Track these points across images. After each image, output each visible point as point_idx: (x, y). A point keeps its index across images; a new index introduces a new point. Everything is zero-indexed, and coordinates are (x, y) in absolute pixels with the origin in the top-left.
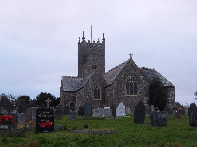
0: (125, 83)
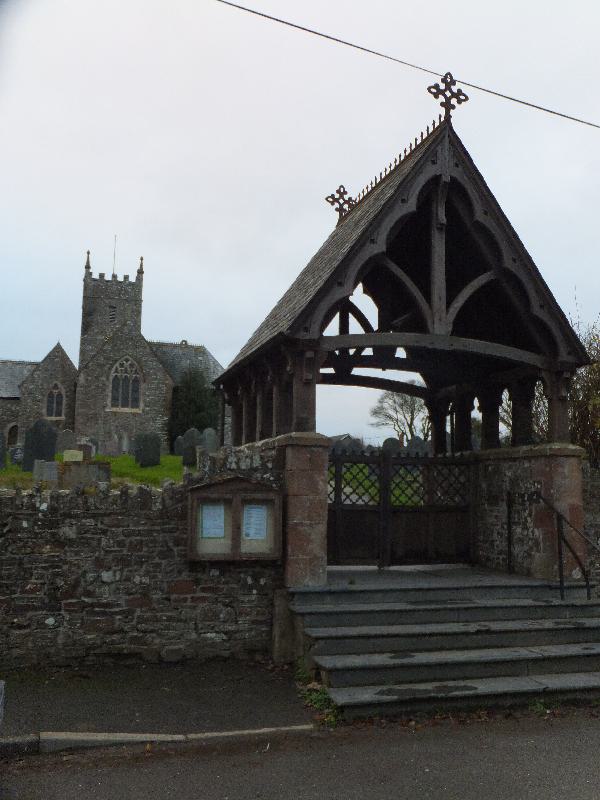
0: (108, 379)
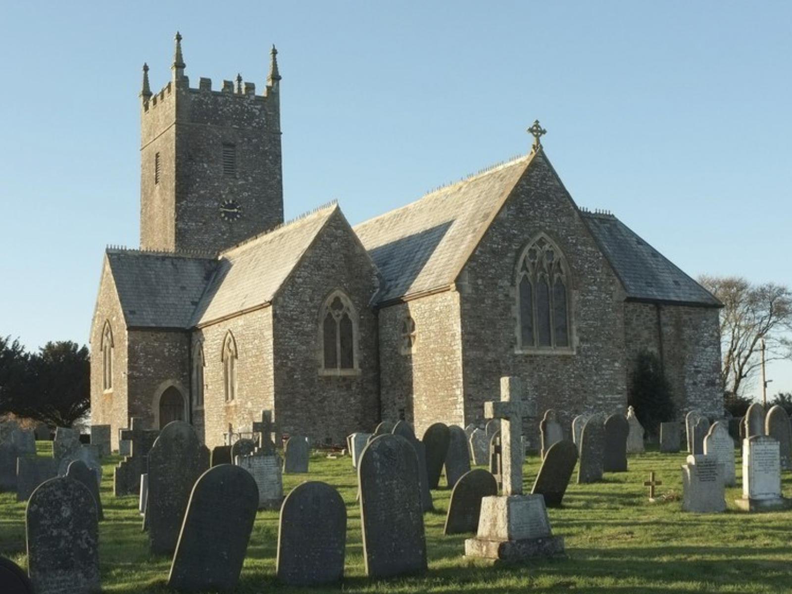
0: (513, 284)
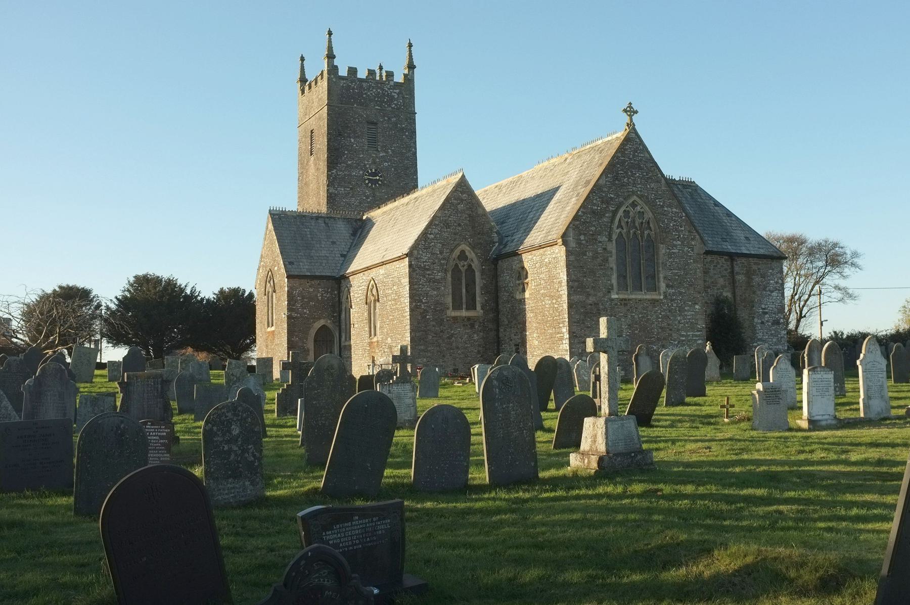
0: (610, 240)
